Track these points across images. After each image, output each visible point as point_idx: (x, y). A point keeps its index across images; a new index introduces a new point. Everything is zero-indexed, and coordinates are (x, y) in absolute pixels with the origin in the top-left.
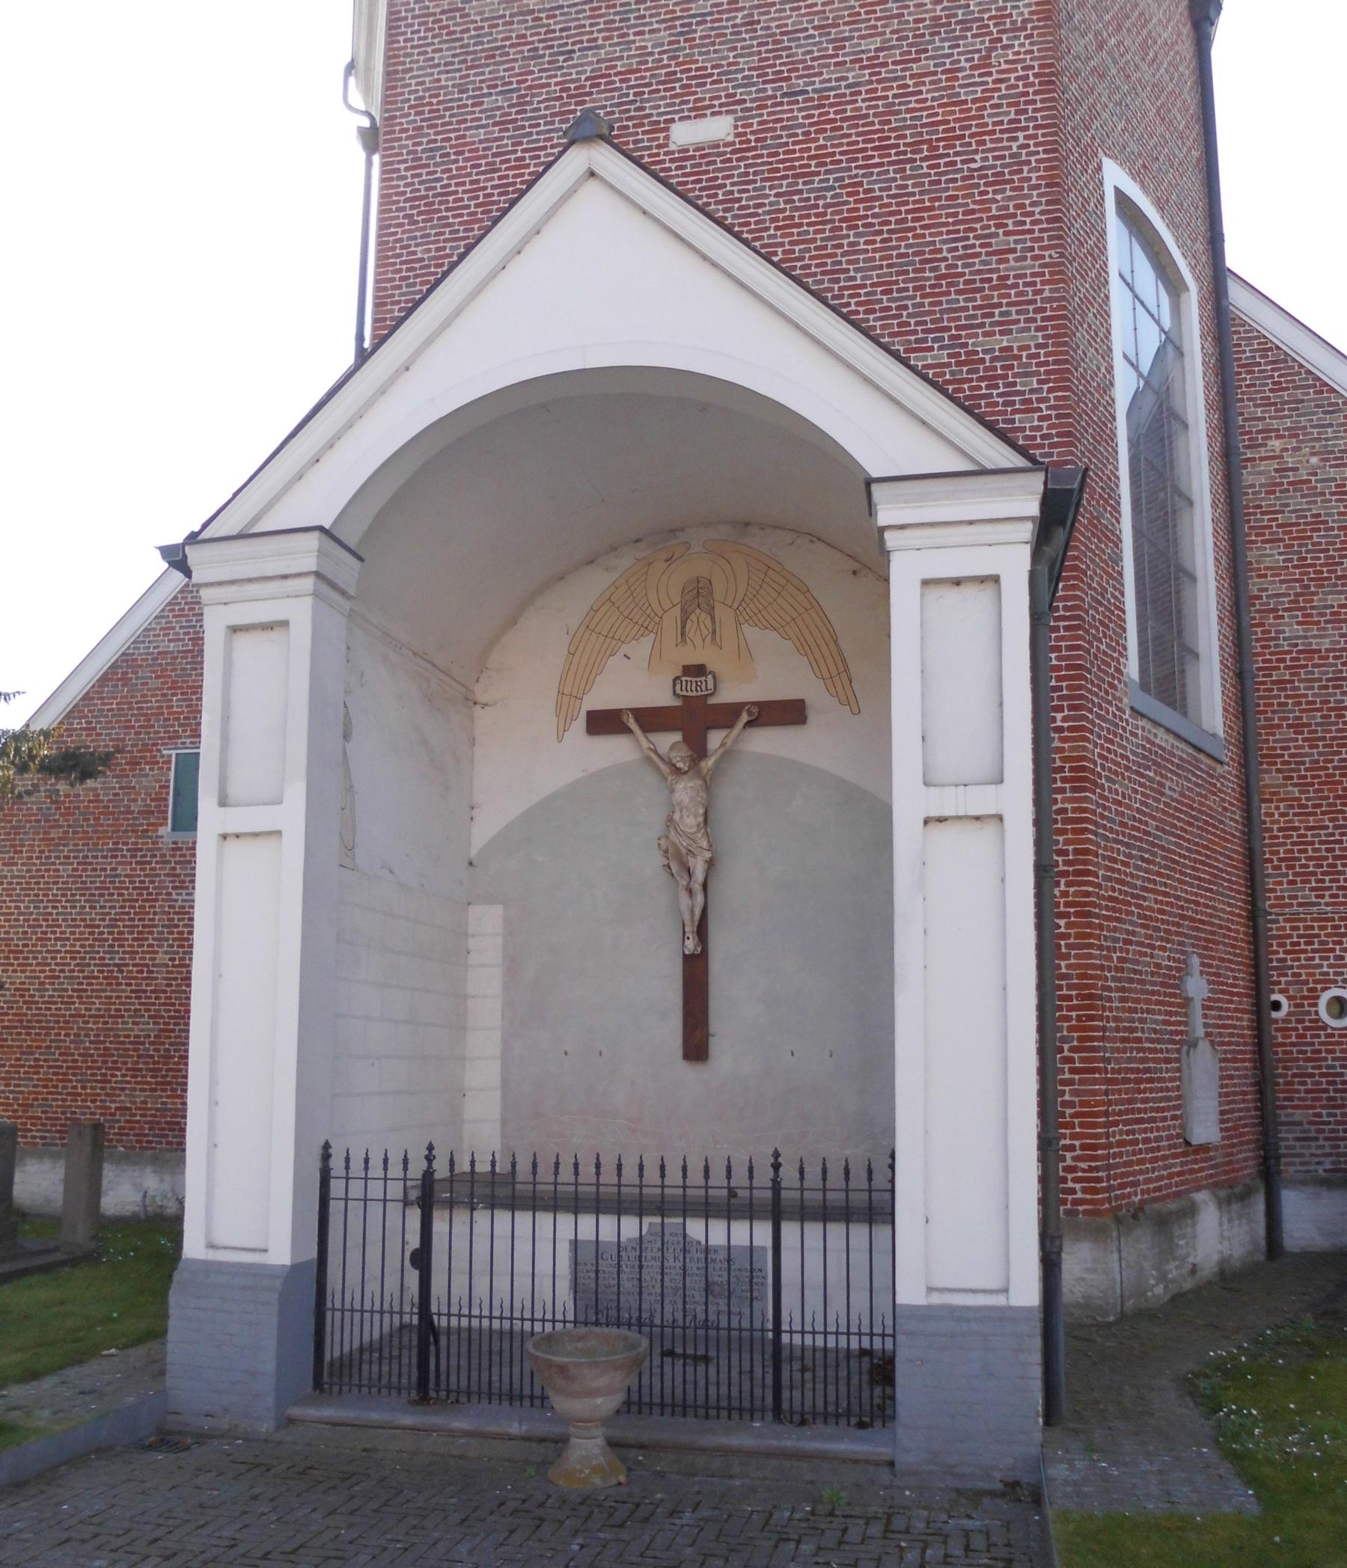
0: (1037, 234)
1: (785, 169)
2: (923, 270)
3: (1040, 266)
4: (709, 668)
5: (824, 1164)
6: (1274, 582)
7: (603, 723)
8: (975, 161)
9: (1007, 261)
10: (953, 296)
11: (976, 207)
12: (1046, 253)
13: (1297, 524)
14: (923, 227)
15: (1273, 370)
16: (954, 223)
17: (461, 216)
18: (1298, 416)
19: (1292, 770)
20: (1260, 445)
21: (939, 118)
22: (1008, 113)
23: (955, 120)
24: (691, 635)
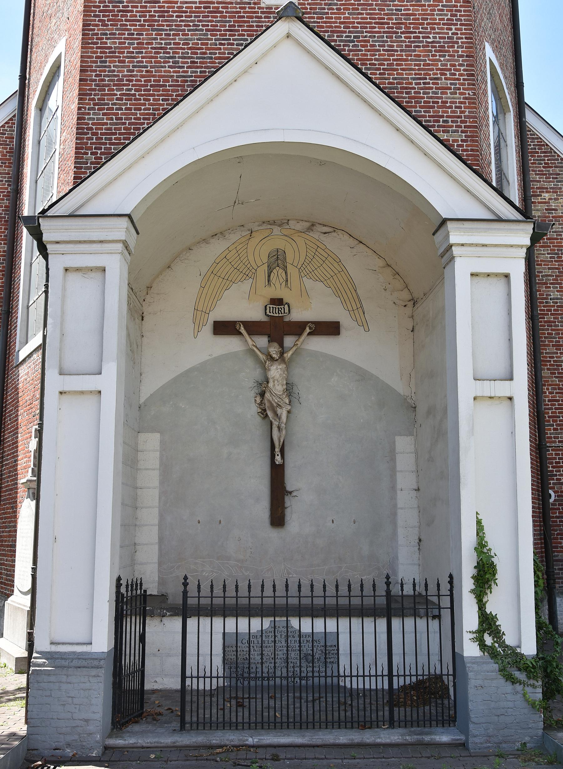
0: (462, 81)
1: (327, 27)
2: (402, 93)
3: (463, 98)
4: (285, 301)
5: (287, 582)
6: (545, 269)
7: (223, 328)
8: (430, 38)
9: (447, 93)
10: (418, 109)
11: (431, 62)
12: (467, 92)
13: (557, 239)
14: (402, 69)
15: (544, 156)
16: (419, 70)
17: (136, 25)
18: (557, 182)
19: (555, 369)
20: (538, 196)
21: (411, 12)
22: (447, 15)
23: (419, 14)
24: (274, 281)
